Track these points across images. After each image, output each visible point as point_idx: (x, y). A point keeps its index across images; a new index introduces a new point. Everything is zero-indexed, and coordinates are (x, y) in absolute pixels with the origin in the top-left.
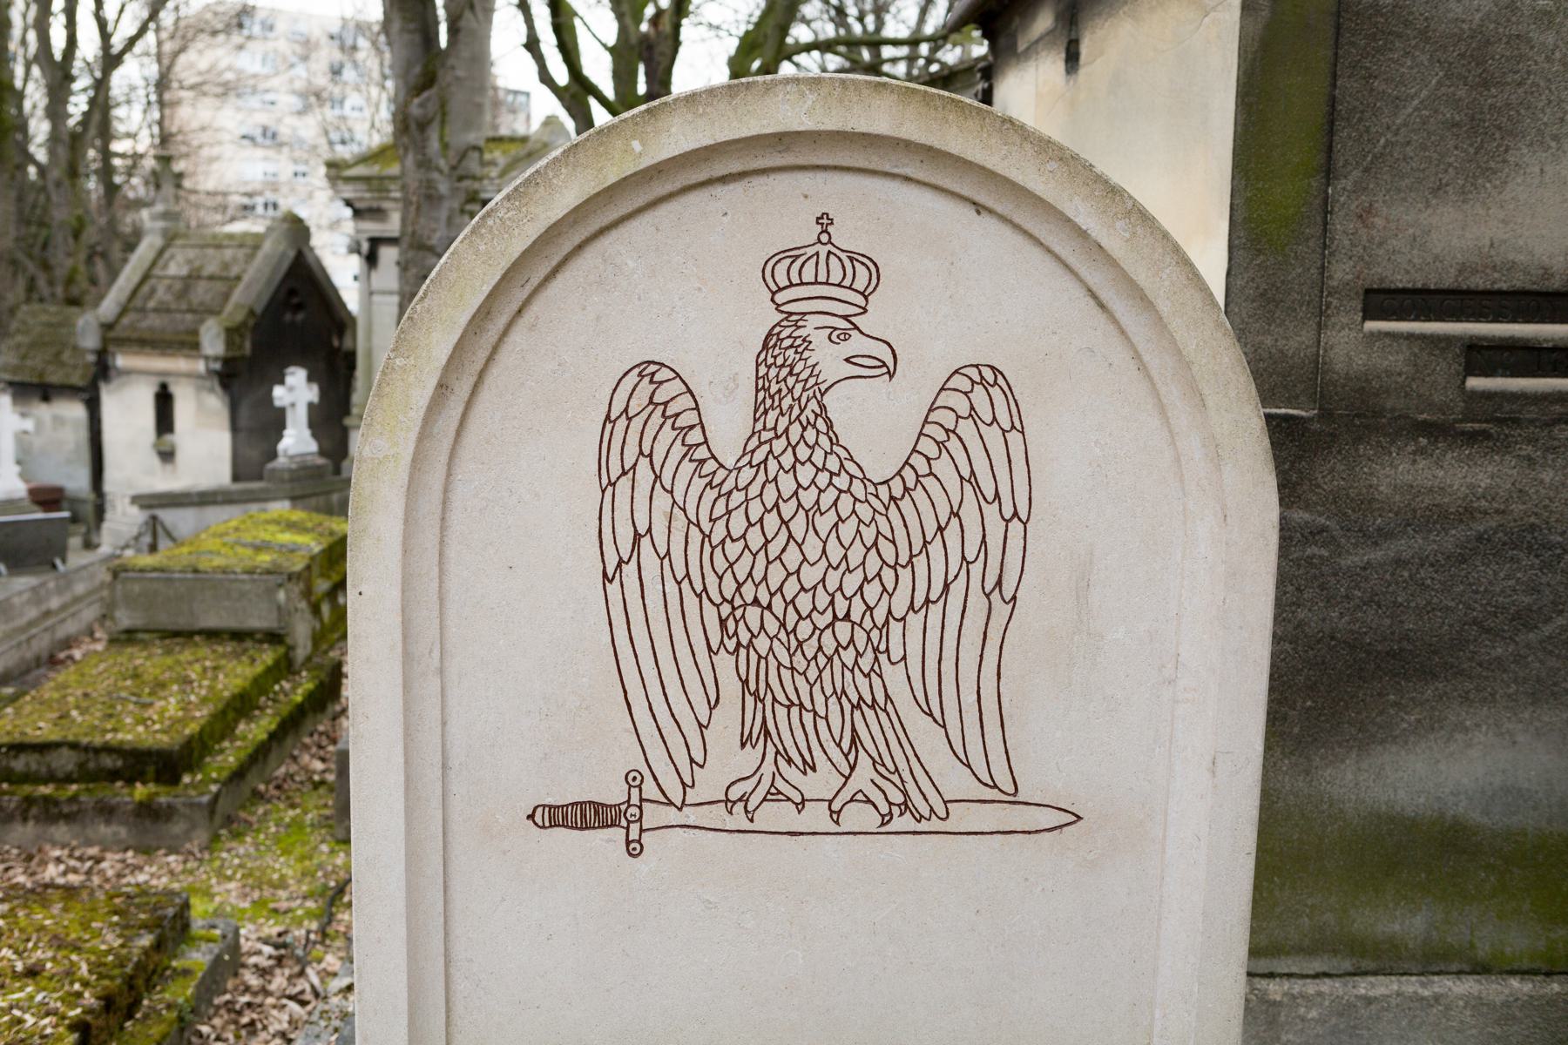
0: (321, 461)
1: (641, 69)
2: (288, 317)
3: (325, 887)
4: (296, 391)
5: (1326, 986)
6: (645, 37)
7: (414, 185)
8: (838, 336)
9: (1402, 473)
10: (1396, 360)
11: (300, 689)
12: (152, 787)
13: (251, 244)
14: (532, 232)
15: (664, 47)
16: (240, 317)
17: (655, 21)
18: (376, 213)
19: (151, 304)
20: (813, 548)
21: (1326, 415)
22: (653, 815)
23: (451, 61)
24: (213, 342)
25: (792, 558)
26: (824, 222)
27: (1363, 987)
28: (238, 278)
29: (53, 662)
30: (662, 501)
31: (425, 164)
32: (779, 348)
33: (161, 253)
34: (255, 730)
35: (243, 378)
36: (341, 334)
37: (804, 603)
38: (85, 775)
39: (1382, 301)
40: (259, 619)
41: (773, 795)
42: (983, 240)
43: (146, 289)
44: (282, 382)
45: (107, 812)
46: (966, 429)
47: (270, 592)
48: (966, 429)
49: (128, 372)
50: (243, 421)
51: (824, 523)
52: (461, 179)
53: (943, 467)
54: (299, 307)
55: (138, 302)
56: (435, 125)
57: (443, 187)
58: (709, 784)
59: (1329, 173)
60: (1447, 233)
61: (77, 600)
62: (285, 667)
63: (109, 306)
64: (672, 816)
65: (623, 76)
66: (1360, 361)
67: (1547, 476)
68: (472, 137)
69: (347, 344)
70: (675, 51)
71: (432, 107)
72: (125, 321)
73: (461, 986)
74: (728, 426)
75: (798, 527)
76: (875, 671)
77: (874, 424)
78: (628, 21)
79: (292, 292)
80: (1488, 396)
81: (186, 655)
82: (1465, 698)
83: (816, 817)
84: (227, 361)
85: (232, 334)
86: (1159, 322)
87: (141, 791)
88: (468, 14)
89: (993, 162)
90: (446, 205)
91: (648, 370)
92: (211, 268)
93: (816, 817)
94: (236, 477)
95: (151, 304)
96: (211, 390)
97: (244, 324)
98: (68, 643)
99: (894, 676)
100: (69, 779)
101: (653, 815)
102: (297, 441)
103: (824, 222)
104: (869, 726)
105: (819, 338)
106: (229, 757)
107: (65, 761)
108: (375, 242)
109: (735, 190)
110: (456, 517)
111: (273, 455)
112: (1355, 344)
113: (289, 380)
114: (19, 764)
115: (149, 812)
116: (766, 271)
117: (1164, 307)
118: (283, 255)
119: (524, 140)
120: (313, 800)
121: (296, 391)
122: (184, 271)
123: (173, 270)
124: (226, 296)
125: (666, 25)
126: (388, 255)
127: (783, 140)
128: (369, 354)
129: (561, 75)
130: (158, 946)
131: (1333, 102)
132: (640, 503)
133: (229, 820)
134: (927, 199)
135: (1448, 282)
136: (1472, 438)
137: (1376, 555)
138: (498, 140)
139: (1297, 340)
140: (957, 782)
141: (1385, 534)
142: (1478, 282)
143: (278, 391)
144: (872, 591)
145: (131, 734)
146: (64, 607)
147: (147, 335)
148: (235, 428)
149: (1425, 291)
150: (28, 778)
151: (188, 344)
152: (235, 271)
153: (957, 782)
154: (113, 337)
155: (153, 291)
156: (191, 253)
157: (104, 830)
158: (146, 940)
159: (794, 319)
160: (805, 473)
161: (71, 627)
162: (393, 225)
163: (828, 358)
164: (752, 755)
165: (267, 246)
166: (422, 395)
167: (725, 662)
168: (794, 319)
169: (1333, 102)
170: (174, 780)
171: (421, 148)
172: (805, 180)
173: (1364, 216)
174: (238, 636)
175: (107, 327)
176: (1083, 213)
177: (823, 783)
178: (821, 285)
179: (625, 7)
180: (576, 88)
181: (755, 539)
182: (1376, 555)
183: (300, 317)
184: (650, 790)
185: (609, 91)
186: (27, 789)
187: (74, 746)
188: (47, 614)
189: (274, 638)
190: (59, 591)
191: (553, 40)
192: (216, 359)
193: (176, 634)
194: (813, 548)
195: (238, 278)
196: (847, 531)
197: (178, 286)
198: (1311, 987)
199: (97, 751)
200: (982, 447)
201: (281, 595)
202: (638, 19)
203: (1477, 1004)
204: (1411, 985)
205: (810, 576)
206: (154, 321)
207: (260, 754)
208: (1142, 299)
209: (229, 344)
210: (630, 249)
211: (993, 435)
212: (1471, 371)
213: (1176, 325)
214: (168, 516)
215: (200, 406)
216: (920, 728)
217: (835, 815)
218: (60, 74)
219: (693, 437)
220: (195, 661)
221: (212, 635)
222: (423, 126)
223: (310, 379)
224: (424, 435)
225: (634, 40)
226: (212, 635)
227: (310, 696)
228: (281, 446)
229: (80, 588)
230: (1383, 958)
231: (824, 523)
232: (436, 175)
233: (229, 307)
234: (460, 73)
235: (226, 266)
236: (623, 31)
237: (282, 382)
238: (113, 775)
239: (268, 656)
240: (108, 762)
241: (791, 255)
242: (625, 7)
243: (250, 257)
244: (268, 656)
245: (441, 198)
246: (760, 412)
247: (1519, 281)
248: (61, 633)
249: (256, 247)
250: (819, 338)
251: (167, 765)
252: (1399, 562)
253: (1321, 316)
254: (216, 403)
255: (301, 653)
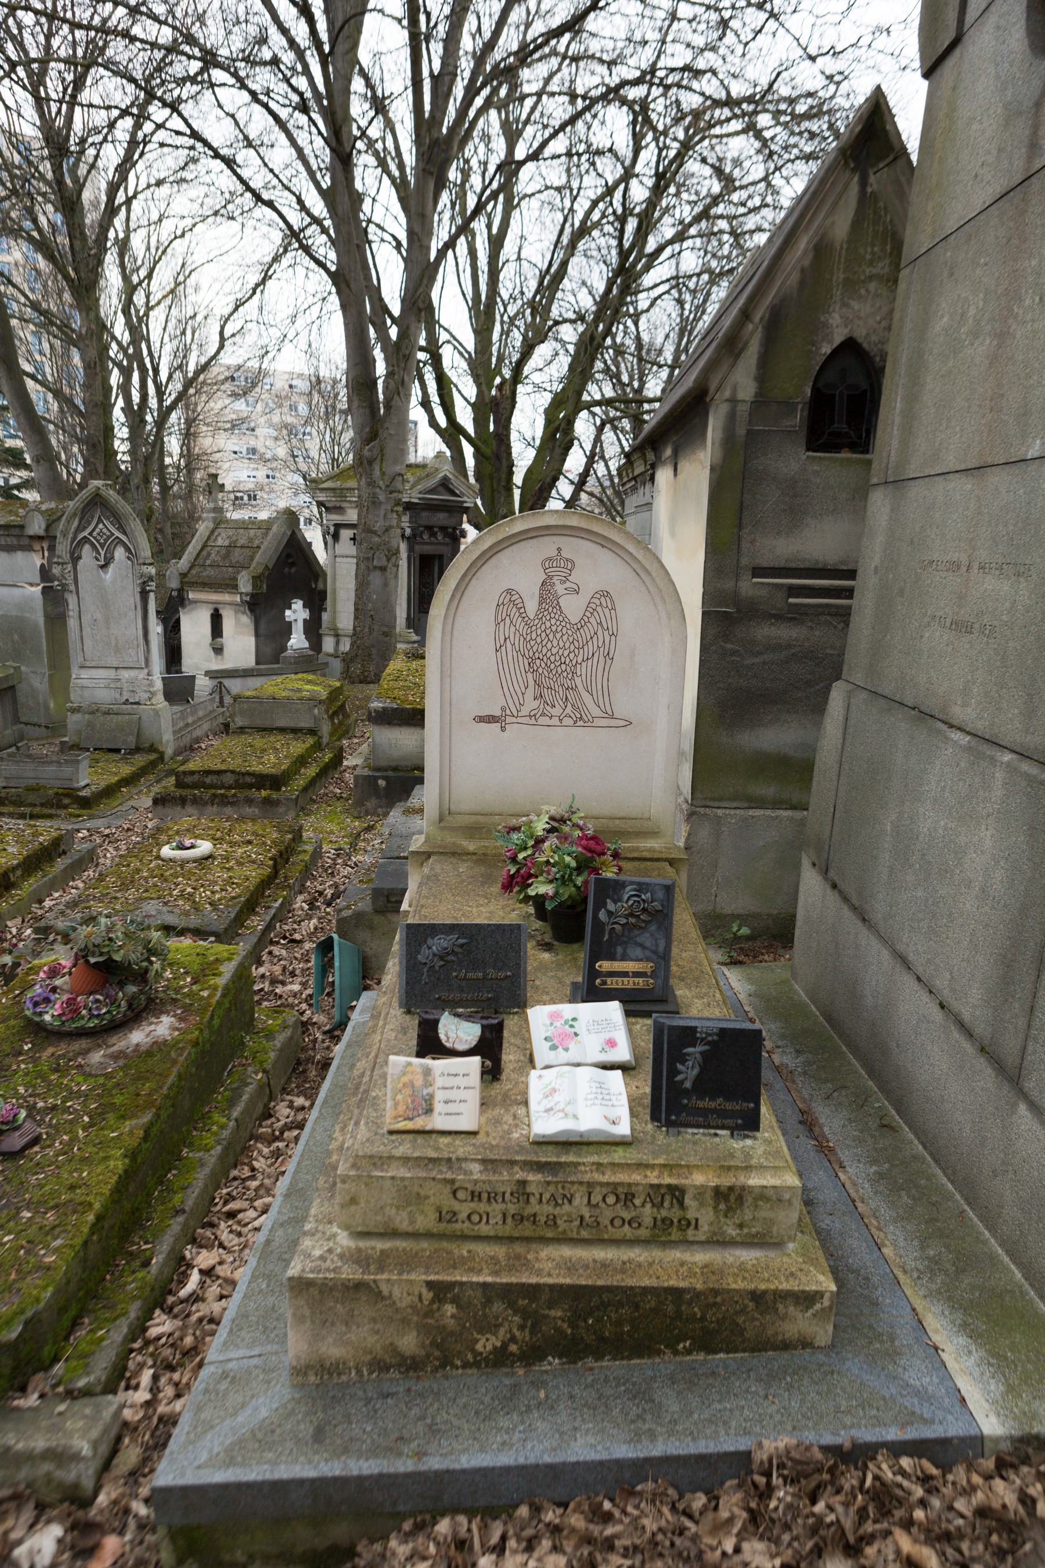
0: (311, 653)
1: (427, 115)
2: (286, 570)
3: (352, 834)
4: (297, 613)
5: (738, 812)
6: (495, 397)
7: (365, 496)
8: (563, 582)
9: (766, 632)
10: (764, 592)
11: (328, 756)
12: (269, 792)
13: (266, 526)
14: (478, 553)
15: (506, 404)
16: (260, 570)
17: (500, 387)
18: (339, 510)
19: (208, 562)
20: (555, 643)
21: (739, 611)
22: (509, 719)
23: (386, 425)
24: (245, 585)
25: (549, 645)
26: (559, 550)
27: (751, 812)
28: (259, 547)
29: (192, 749)
30: (513, 629)
31: (371, 484)
32: (546, 585)
33: (212, 532)
34: (311, 771)
35: (263, 608)
36: (316, 582)
37: (552, 658)
38: (238, 786)
39: (758, 571)
40: (305, 723)
41: (543, 714)
42: (604, 556)
43: (204, 553)
44: (290, 608)
45: (250, 801)
46: (599, 609)
47: (311, 709)
48: (599, 609)
49: (196, 602)
50: (262, 631)
51: (558, 636)
52: (391, 492)
53: (592, 620)
54: (293, 564)
55: (200, 561)
56: (378, 461)
57: (382, 498)
58: (525, 711)
59: (740, 527)
60: (780, 548)
61: (200, 719)
62: (318, 746)
63: (184, 563)
64: (514, 720)
65: (479, 421)
66: (750, 593)
67: (817, 633)
68: (398, 468)
69: (320, 586)
70: (513, 407)
71: (375, 452)
72: (193, 572)
73: (453, 768)
74: (532, 607)
75: (551, 636)
76: (573, 679)
77: (573, 607)
78: (484, 387)
79: (288, 556)
80: (796, 605)
81: (272, 739)
82: (788, 711)
83: (555, 721)
84: (252, 596)
85: (256, 580)
86: (653, 579)
87: (264, 793)
88: (396, 397)
89: (606, 534)
90: (383, 507)
91: (509, 591)
92: (242, 542)
93: (555, 721)
94: (257, 663)
95: (208, 562)
96: (244, 613)
97: (262, 574)
98: (198, 740)
99: (578, 680)
100: (230, 787)
101: (509, 719)
102: (297, 640)
103: (559, 550)
104: (571, 695)
105: (557, 583)
106: (301, 782)
107: (229, 779)
108: (338, 526)
109: (534, 541)
110: (455, 633)
111: (284, 648)
112: (749, 586)
113: (294, 606)
114: (208, 780)
115: (267, 802)
116: (543, 564)
117: (654, 574)
118: (284, 533)
119: (424, 466)
120: (338, 804)
121: (297, 613)
122: (227, 543)
123: (220, 542)
124: (252, 558)
125: (507, 387)
126: (346, 534)
127: (548, 527)
128: (334, 591)
129: (442, 421)
130: (294, 839)
131: (742, 503)
132: (507, 629)
133: (303, 809)
134: (588, 543)
135: (782, 565)
136: (791, 619)
137: (756, 660)
138: (410, 466)
139: (729, 585)
140: (596, 712)
141: (760, 653)
142: (793, 565)
143: (288, 613)
144: (572, 655)
145: (257, 768)
146: (194, 722)
147: (206, 580)
148: (257, 635)
149: (773, 568)
150: (216, 787)
151: (231, 586)
152: (256, 543)
153: (596, 712)
154: (187, 581)
155: (209, 554)
156: (230, 532)
157: (248, 810)
158: (290, 836)
159: (550, 577)
160: (553, 621)
161: (199, 733)
162: (352, 515)
163: (560, 588)
164: (537, 702)
165: (275, 528)
166: (447, 598)
167: (530, 675)
168: (550, 577)
169: (742, 503)
170: (279, 789)
171: (370, 474)
172: (554, 538)
173: (753, 542)
174: (295, 731)
175: (183, 575)
176: (631, 548)
177: (557, 711)
178: (558, 568)
179: (482, 380)
180: (452, 430)
181: (539, 640)
182: (756, 660)
183: (293, 570)
184: (508, 712)
185: (470, 429)
186: (213, 791)
187: (233, 772)
188: (187, 725)
189: (312, 732)
190: (192, 714)
191: (438, 401)
192: (247, 594)
193: (265, 730)
194: (555, 643)
195: (259, 547)
196: (565, 638)
197: (224, 551)
198: (733, 812)
199: (243, 774)
200: (603, 614)
201: (316, 711)
202: (490, 386)
203: (791, 819)
204: (768, 812)
205: (554, 651)
206: (210, 572)
207: (313, 782)
208: (649, 573)
209: (255, 586)
210: (504, 558)
211: (607, 611)
212: (790, 596)
213: (657, 579)
214: (227, 682)
215: (237, 620)
216: (585, 695)
217: (561, 720)
218: (137, 419)
219: (521, 609)
220: (278, 740)
221: (282, 730)
222: (370, 462)
223: (304, 606)
224: (448, 609)
225: (487, 400)
226: (282, 730)
227: (331, 760)
228: (289, 644)
229: (201, 713)
230: (759, 803)
231: (558, 636)
232: (378, 490)
233: (253, 565)
234: (392, 432)
235: (251, 540)
236: (480, 394)
237: (290, 608)
238: (250, 786)
239: (310, 741)
240: (248, 779)
241: (550, 559)
242: (482, 380)
243: (266, 534)
244: (310, 741)
245: (380, 503)
246: (540, 603)
247: (807, 565)
248: (194, 736)
249: (269, 529)
250: (557, 583)
251: (275, 782)
252: (764, 663)
253: (737, 577)
254: (246, 620)
255: (325, 740)
